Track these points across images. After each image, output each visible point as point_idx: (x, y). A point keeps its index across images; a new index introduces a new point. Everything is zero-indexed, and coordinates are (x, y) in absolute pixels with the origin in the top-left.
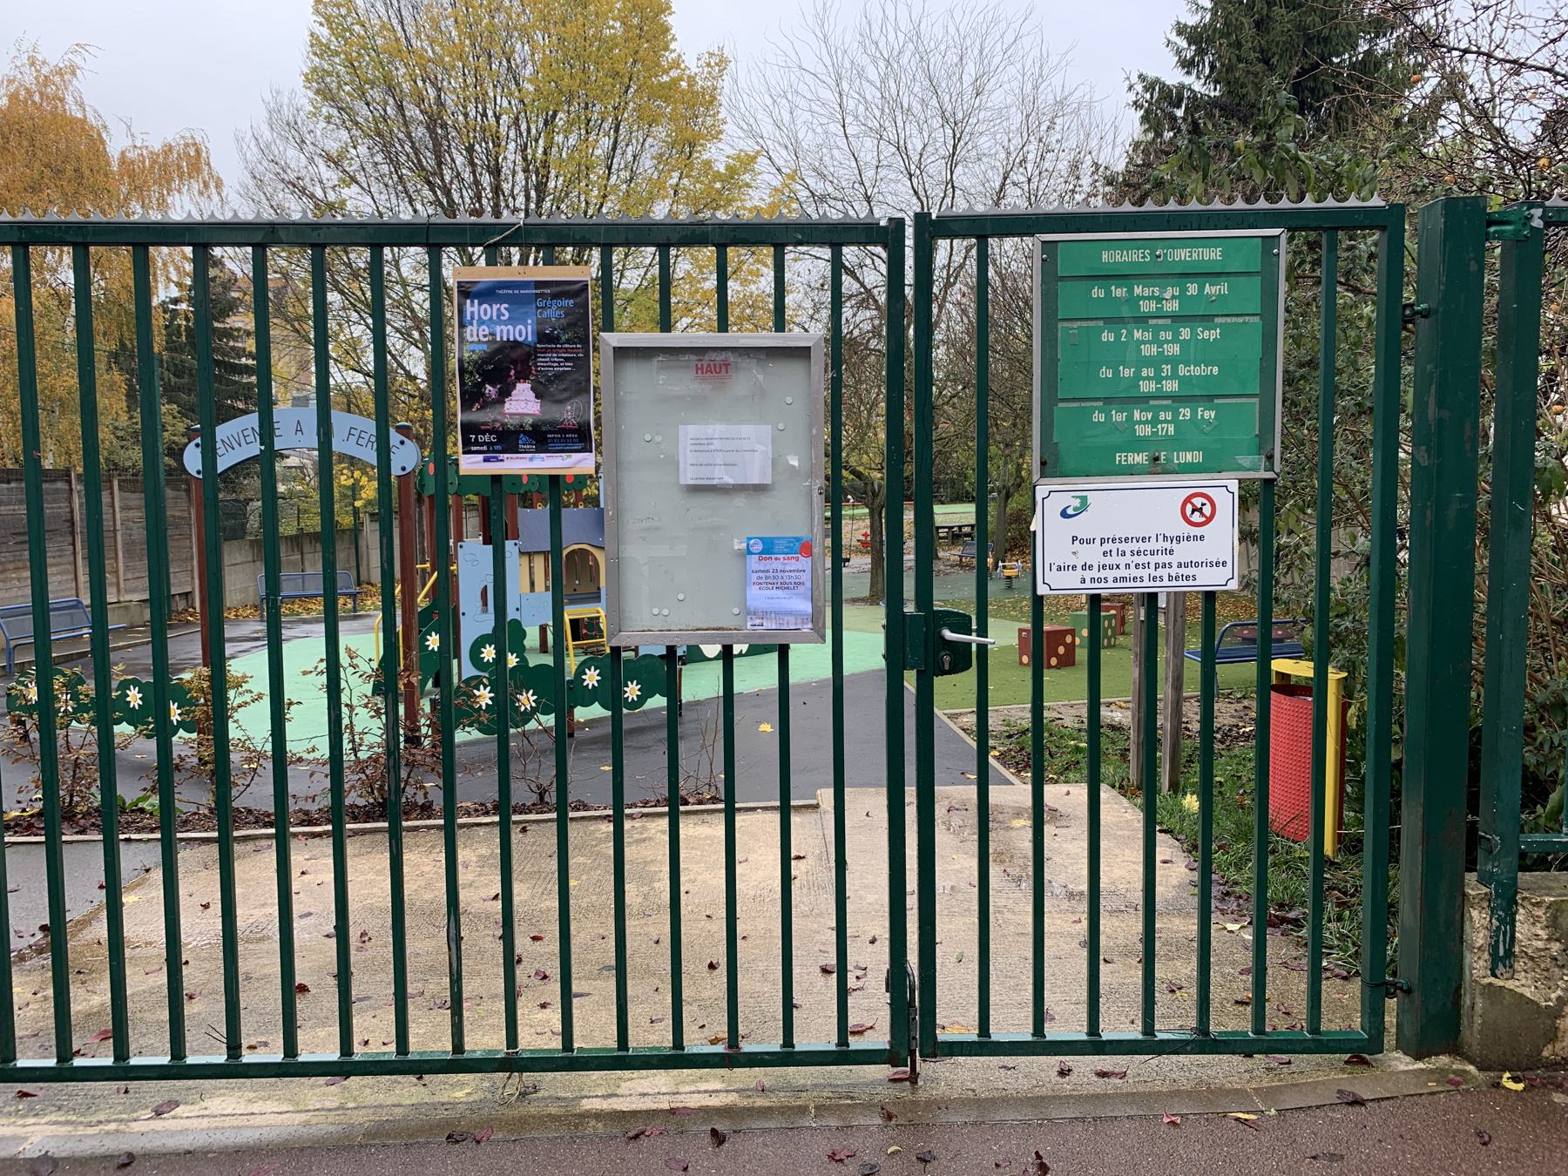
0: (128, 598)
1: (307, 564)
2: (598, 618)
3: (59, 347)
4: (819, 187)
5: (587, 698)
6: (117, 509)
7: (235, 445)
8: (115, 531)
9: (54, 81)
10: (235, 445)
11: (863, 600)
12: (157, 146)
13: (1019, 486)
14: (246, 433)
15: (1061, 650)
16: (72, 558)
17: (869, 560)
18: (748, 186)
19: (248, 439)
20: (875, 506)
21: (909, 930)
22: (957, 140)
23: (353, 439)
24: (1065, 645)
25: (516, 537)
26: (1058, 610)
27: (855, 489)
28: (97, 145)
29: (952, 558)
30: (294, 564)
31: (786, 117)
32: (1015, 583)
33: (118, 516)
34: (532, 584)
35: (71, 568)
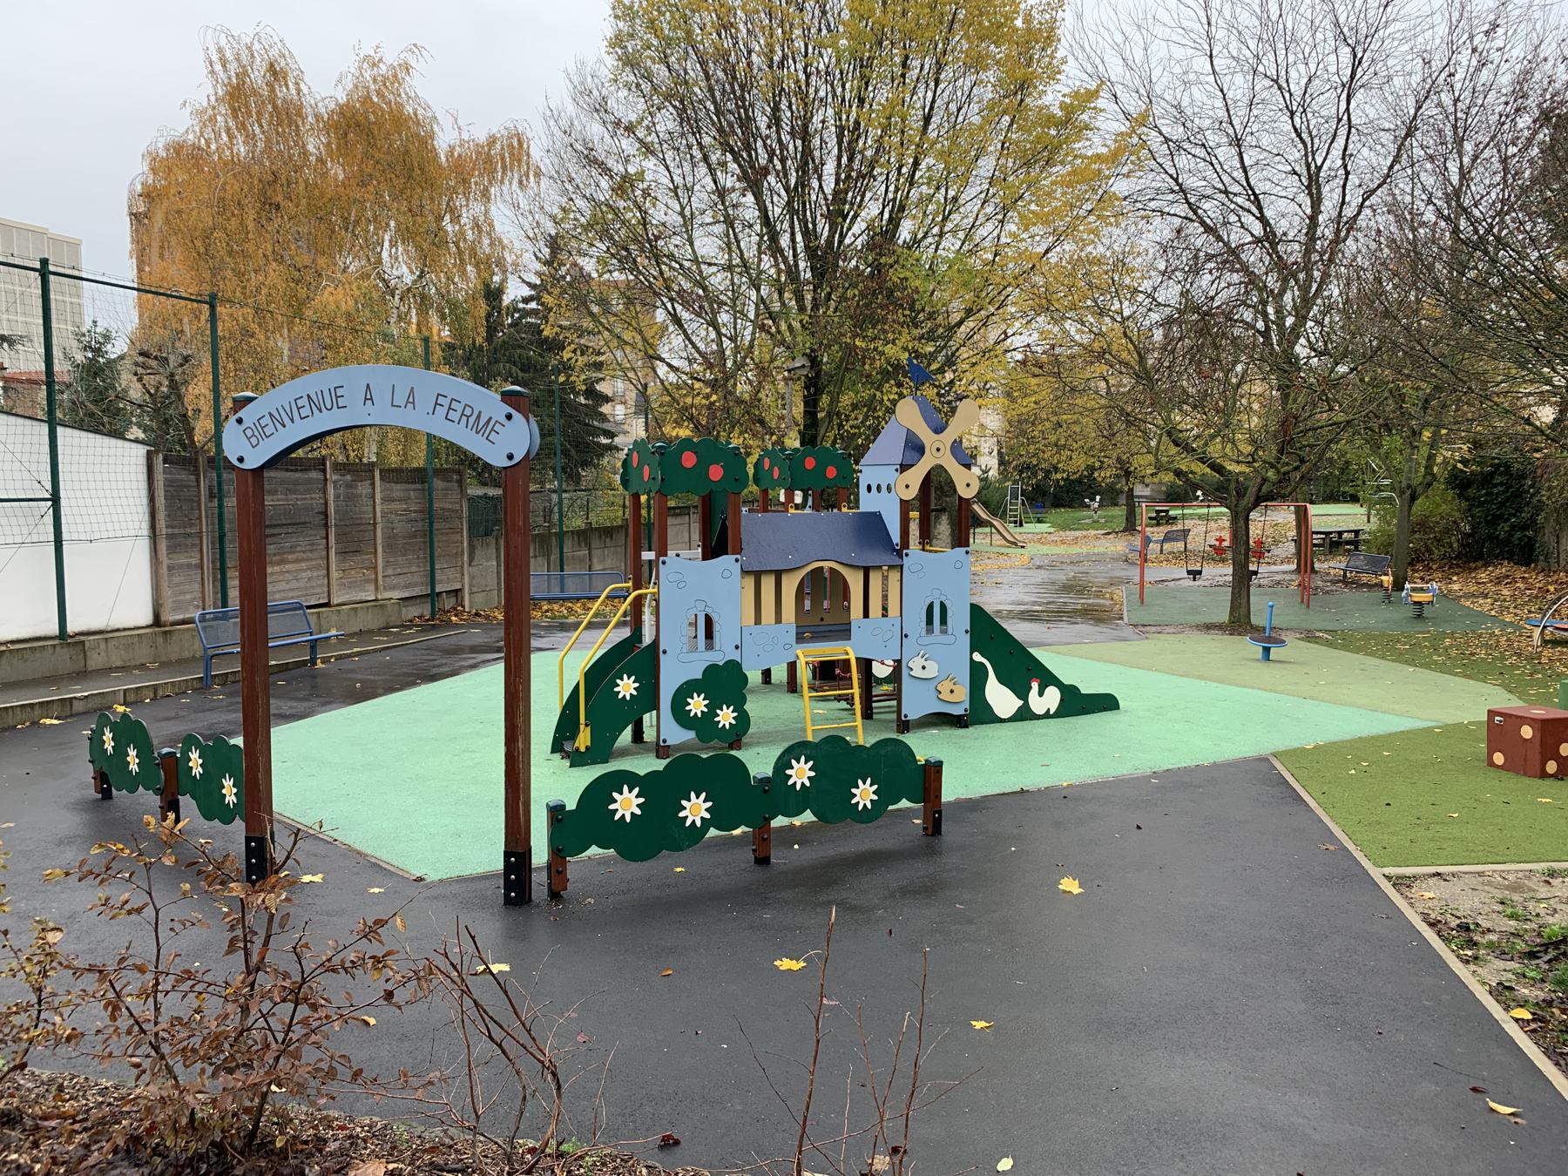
0: (387, 595)
1: (595, 560)
2: (848, 660)
4: (1177, 133)
5: (795, 801)
6: (378, 501)
7: (287, 421)
8: (375, 524)
9: (393, 79)
10: (287, 421)
11: (1219, 627)
12: (482, 138)
13: (1429, 485)
14: (300, 403)
16: (324, 553)
17: (1230, 570)
18: (1087, 127)
19: (304, 412)
22: (1356, 63)
23: (441, 411)
25: (739, 550)
26: (1503, 658)
28: (425, 142)
29: (1332, 572)
30: (581, 560)
31: (1139, 54)
32: (1427, 611)
33: (378, 509)
35: (323, 563)
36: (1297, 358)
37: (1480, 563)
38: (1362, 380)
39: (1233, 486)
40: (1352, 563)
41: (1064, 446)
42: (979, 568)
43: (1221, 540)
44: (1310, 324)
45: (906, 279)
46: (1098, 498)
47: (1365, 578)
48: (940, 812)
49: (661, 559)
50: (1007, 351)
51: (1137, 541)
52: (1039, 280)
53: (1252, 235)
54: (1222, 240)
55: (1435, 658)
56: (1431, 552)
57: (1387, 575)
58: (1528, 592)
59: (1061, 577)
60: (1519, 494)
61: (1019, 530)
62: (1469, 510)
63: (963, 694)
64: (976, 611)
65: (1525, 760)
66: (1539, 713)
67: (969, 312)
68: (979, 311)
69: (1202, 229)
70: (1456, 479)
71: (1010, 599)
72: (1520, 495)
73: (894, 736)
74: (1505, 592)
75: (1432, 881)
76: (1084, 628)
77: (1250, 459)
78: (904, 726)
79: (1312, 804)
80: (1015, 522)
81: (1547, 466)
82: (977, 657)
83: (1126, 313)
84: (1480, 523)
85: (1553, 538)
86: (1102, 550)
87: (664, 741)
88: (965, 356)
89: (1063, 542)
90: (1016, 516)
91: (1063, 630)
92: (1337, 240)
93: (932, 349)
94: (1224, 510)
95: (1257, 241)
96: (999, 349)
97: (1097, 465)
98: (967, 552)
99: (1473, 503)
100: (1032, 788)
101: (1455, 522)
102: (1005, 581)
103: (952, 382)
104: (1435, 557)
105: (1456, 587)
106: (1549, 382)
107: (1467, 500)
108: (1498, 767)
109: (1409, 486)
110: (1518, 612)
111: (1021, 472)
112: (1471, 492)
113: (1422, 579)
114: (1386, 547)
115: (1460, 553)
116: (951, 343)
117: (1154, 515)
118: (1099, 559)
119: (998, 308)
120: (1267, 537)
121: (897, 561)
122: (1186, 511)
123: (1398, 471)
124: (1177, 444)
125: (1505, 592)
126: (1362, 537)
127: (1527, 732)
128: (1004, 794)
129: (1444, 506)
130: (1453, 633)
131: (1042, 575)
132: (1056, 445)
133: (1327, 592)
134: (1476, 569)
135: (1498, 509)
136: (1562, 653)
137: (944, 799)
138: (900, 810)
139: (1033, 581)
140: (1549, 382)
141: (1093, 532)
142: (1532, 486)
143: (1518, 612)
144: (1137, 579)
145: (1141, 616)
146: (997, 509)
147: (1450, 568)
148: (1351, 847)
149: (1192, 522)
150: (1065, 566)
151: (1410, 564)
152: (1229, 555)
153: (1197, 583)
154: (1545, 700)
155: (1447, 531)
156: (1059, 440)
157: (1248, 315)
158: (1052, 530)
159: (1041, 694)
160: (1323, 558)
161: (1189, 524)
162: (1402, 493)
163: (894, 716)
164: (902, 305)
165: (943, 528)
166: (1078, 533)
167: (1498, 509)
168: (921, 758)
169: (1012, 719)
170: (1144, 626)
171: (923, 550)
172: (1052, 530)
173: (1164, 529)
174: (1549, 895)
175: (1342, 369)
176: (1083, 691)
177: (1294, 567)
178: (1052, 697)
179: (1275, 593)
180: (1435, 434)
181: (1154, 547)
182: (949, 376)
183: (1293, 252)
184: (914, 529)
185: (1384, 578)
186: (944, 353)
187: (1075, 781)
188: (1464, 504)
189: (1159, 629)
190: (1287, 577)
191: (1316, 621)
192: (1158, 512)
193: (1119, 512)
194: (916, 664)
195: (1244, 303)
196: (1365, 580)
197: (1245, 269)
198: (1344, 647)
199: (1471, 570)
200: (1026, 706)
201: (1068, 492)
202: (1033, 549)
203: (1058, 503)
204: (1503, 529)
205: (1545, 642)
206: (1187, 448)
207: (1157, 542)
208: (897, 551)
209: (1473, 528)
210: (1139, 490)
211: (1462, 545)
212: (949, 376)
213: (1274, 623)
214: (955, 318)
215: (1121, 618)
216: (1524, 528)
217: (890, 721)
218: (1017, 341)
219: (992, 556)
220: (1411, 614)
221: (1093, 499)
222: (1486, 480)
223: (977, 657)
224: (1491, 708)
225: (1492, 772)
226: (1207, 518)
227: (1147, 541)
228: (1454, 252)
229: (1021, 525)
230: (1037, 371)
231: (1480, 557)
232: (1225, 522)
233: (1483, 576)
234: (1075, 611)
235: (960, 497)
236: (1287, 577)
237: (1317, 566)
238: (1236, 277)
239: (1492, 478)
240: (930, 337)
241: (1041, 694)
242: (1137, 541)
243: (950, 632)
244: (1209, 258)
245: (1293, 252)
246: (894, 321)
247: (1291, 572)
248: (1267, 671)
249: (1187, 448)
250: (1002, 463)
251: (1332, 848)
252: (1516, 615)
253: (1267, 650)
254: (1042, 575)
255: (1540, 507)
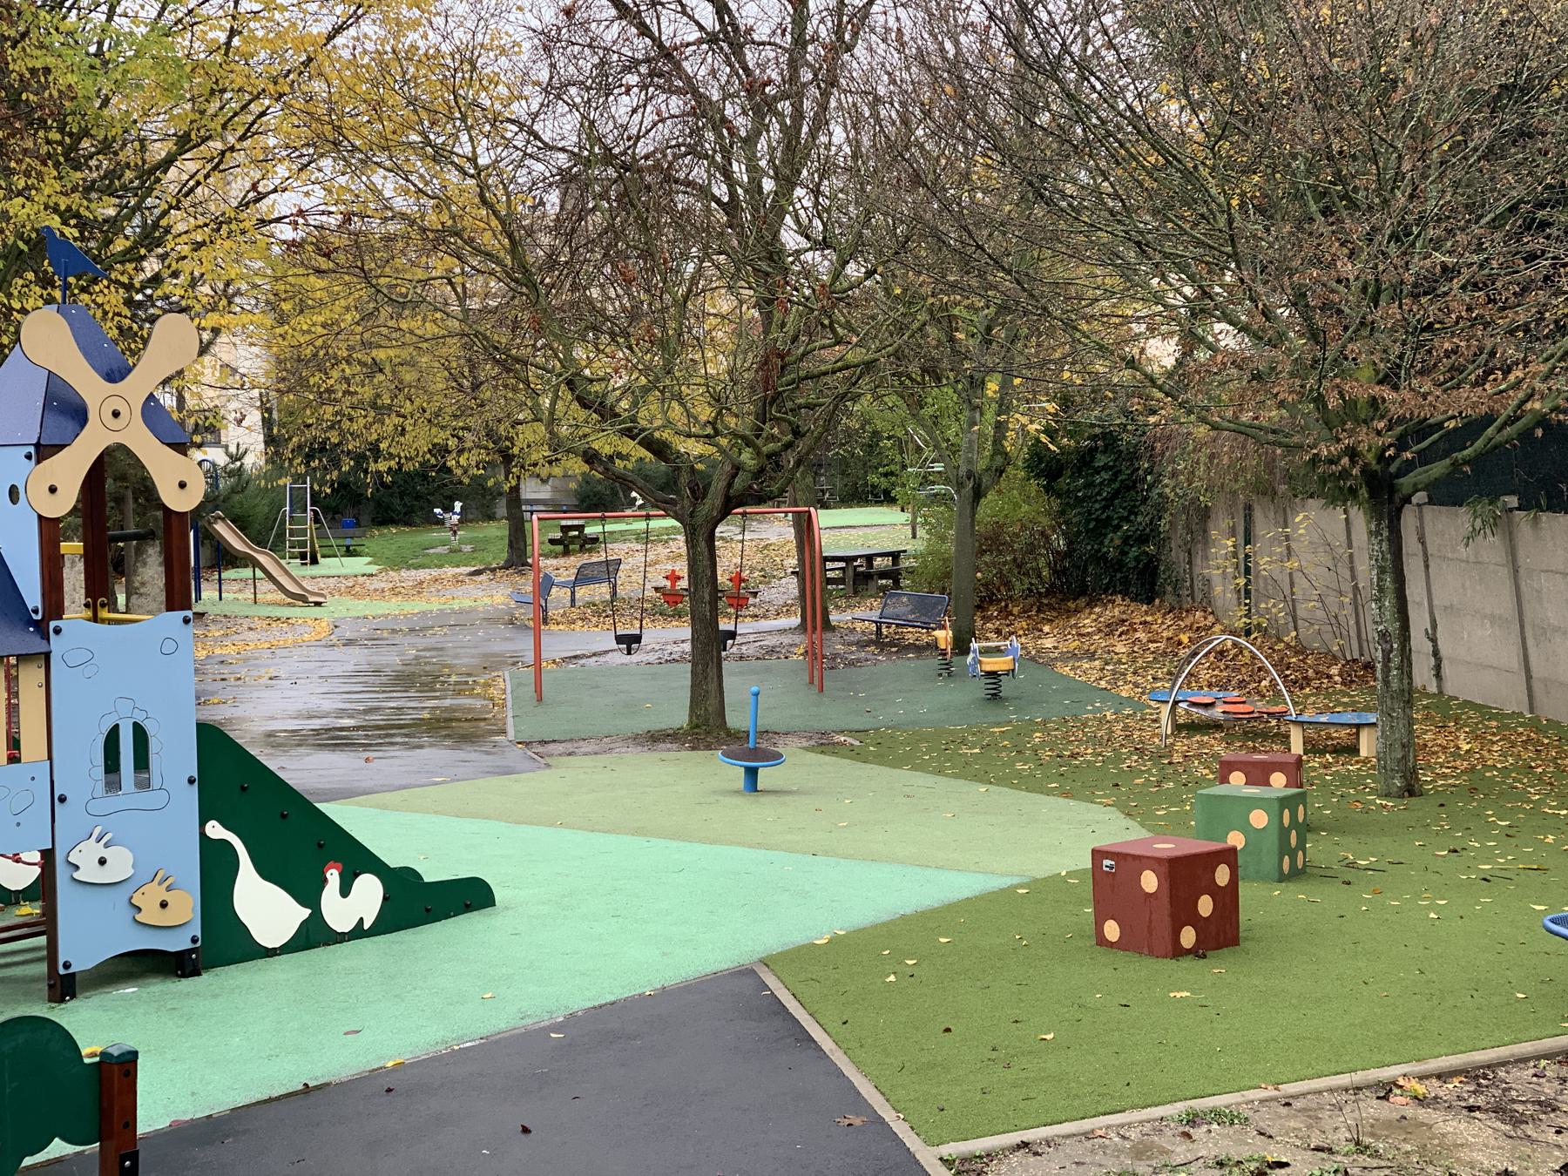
3: (1420, 604)
13: (1000, 471)
15: (1205, 906)
17: (686, 632)
20: (699, 520)
21: (67, 587)
24: (1214, 890)
26: (1118, 759)
27: (646, 478)
29: (859, 626)
34: (14, 743)
36: (781, 251)
37: (1082, 601)
38: (888, 291)
39: (684, 479)
40: (889, 611)
41: (390, 407)
42: (231, 650)
43: (673, 577)
44: (799, 192)
45: (47, 70)
46: (458, 506)
47: (911, 636)
48: (134, 1156)
49: (53, 624)
50: (263, 222)
51: (527, 585)
52: (318, 86)
53: (701, 28)
54: (650, 35)
55: (1019, 766)
56: (1008, 585)
57: (943, 627)
58: (1152, 646)
59: (391, 659)
60: (1131, 485)
61: (311, 570)
62: (1062, 513)
63: (186, 908)
64: (212, 741)
65: (1150, 930)
66: (1166, 848)
67: (184, 143)
68: (205, 140)
69: (613, 12)
70: (1040, 461)
71: (292, 708)
72: (1134, 487)
73: (41, 1010)
74: (1121, 648)
75: (1015, 1159)
76: (434, 755)
77: (709, 430)
78: (64, 987)
79: (826, 1044)
80: (303, 556)
81: (1169, 438)
82: (215, 830)
83: (483, 161)
84: (1079, 533)
85: (1183, 556)
86: (467, 603)
87: (67, 965)
88: (181, 227)
89: (395, 592)
90: (303, 544)
91: (395, 762)
92: (840, 46)
93: (112, 212)
94: (671, 522)
95: (712, 39)
96: (250, 216)
97: (452, 443)
98: (186, 621)
99: (1069, 500)
100: (334, 1079)
101: (1042, 533)
102: (282, 674)
103: (156, 280)
104: (1017, 593)
105: (1048, 643)
106: (1158, 299)
107: (1059, 496)
108: (1112, 945)
109: (970, 475)
110: (1140, 680)
111: (309, 457)
112: (1063, 482)
113: (998, 632)
114: (941, 579)
115: (1052, 585)
116: (149, 201)
117: (558, 535)
118: (461, 621)
119: (242, 138)
120: (752, 569)
121: (37, 645)
122: (608, 528)
123: (954, 449)
124: (585, 404)
125: (1121, 648)
126: (905, 563)
127: (1149, 882)
128: (270, 1100)
129: (1025, 508)
130: (1045, 722)
131: (355, 658)
132: (374, 405)
133: (852, 664)
134: (1077, 611)
135: (1105, 508)
136: (1202, 744)
137: (142, 1128)
138: (50, 1163)
139: (338, 671)
140: (1158, 299)
141: (450, 571)
142: (1149, 471)
143: (1140, 680)
144: (530, 657)
145: (532, 731)
146: (266, 532)
147: (1039, 611)
148: (888, 1115)
149: (625, 547)
150: (398, 639)
151: (978, 607)
152: (685, 605)
153: (634, 658)
154: (1177, 824)
155: (1031, 549)
156: (378, 396)
157: (699, 173)
158: (373, 569)
159: (345, 891)
160: (842, 603)
161: (616, 550)
162: (960, 486)
163: (43, 968)
164: (42, 121)
165: (152, 571)
166: (423, 574)
167: (1105, 508)
168: (90, 1046)
169: (292, 947)
170: (543, 742)
171: (95, 619)
172: (373, 569)
173: (575, 561)
174: (1190, 1157)
175: (853, 270)
176: (429, 877)
177: (795, 621)
178: (369, 894)
179: (768, 670)
180: (1005, 386)
181: (559, 595)
182: (151, 266)
183: (767, 63)
184: (74, 579)
185: (939, 634)
186: (137, 221)
187: (406, 1057)
188: (1056, 504)
189: (569, 747)
190: (786, 640)
191: (834, 714)
192: (565, 529)
193: (497, 531)
194: (85, 858)
195: (692, 151)
196: (910, 638)
197: (691, 88)
198: (880, 759)
199: (1070, 613)
200: (317, 917)
201: (402, 495)
202: (339, 607)
203: (385, 516)
204: (1111, 543)
205: (1178, 728)
206: (606, 412)
207: (563, 585)
208: (36, 624)
209: (1070, 543)
210: (531, 490)
211: (1055, 572)
212: (151, 266)
213: (765, 722)
214: (159, 151)
215: (504, 732)
216: (1143, 540)
217: (34, 980)
218: (284, 204)
219: (258, 624)
220: (982, 694)
221: (448, 509)
222: (1085, 460)
223: (215, 830)
224: (1097, 845)
225: (1104, 956)
226: (646, 538)
227: (545, 586)
228: (1015, 80)
229: (314, 561)
230: (324, 263)
231: (1082, 591)
232: (680, 544)
233: (1087, 622)
234: (418, 724)
235: (167, 511)
236: (786, 640)
237: (835, 617)
238: (675, 104)
239: (1093, 459)
240: (108, 185)
241: (345, 891)
242: (527, 585)
243: (156, 783)
244: (632, 65)
245: (767, 63)
246: (25, 151)
247: (792, 630)
248: (755, 812)
249: (606, 412)
250: (270, 440)
251: (857, 1122)
252: (1136, 685)
253: (752, 773)
254: (355, 658)
255: (1160, 509)
